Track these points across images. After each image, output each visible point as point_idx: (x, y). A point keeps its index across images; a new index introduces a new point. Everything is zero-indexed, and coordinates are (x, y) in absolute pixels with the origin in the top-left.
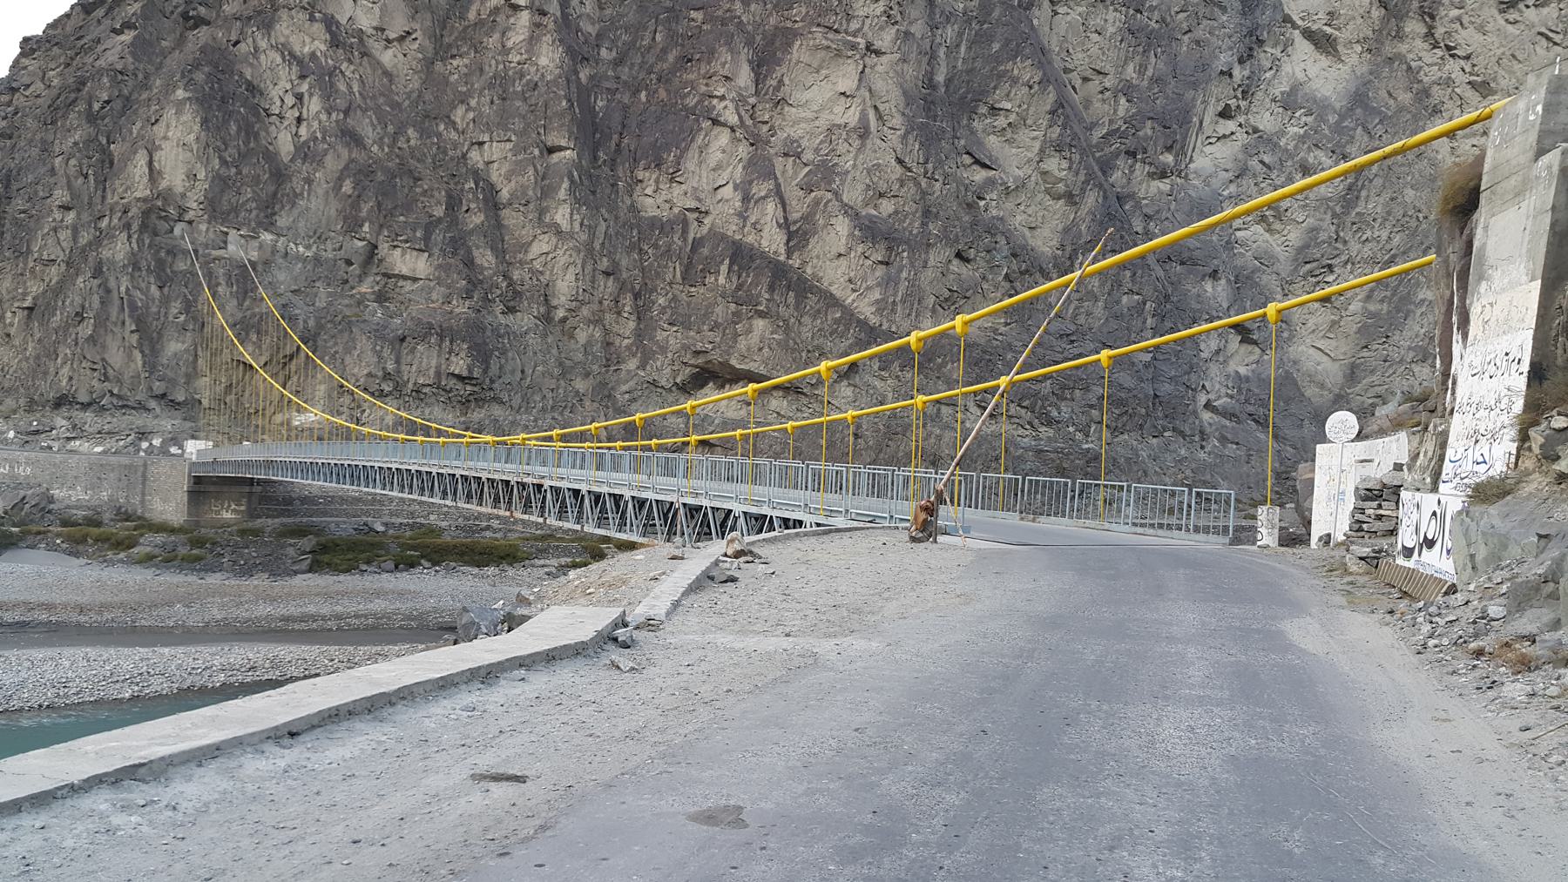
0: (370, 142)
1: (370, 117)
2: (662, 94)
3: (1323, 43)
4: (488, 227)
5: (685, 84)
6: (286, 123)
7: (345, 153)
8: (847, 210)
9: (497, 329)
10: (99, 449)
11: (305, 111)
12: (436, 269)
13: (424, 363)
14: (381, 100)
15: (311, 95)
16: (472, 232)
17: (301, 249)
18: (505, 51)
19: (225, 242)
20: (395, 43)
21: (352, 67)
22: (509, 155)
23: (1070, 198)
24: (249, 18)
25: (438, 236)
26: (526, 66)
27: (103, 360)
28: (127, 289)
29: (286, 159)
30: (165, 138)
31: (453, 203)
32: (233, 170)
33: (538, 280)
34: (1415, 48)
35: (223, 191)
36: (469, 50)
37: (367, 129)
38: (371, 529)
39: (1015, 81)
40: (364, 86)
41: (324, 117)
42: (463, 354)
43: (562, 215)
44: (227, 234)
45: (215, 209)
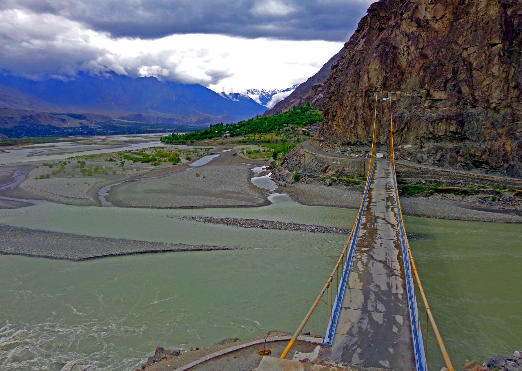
0: (430, 56)
1: (430, 48)
4: (467, 78)
6: (405, 56)
7: (421, 62)
9: (468, 114)
10: (357, 156)
11: (410, 51)
12: (448, 96)
13: (442, 128)
14: (434, 41)
15: (411, 46)
16: (461, 81)
17: (408, 94)
19: (387, 96)
20: (439, 20)
21: (424, 33)
22: (476, 51)
24: (394, 26)
25: (449, 85)
26: (484, 16)
27: (357, 133)
28: (362, 113)
29: (404, 67)
30: (371, 69)
31: (455, 72)
32: (389, 74)
33: (485, 94)
35: (386, 81)
36: (464, 15)
37: (429, 52)
38: (421, 182)
40: (428, 38)
41: (415, 52)
42: (454, 125)
43: (495, 70)
44: (387, 93)
45: (384, 86)
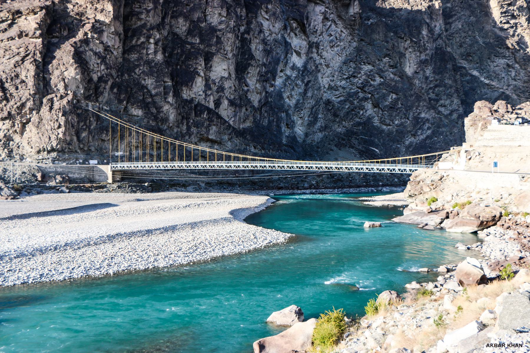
2: (184, 67)
3: (298, 54)
5: (190, 65)
8: (227, 98)
15: (101, 64)
18: (148, 54)
23: (260, 93)
34: (315, 55)
39: (252, 65)
